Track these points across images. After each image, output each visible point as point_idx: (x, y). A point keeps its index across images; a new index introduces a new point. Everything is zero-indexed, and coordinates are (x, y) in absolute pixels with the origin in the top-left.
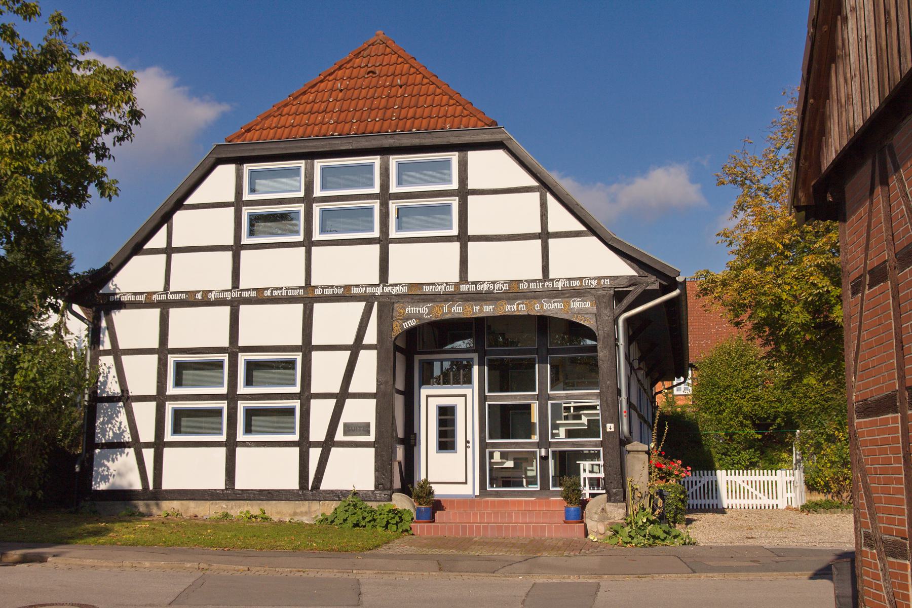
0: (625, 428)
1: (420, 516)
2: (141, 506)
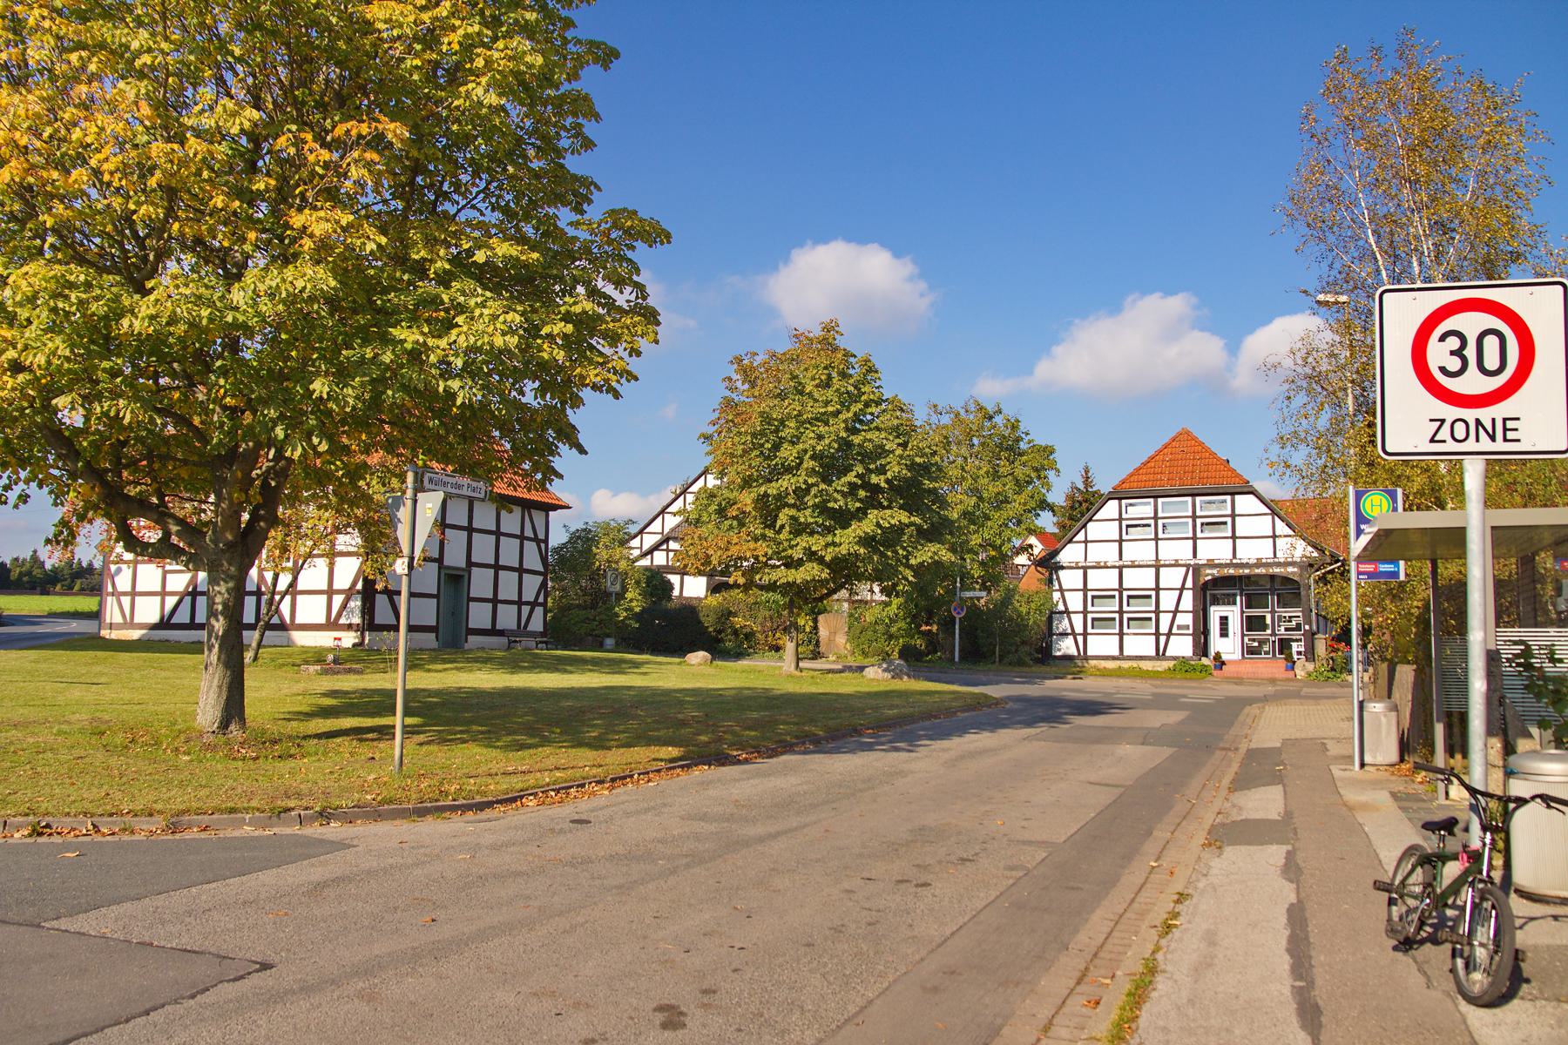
0: (1314, 628)
1: (1215, 666)
2: (1079, 663)
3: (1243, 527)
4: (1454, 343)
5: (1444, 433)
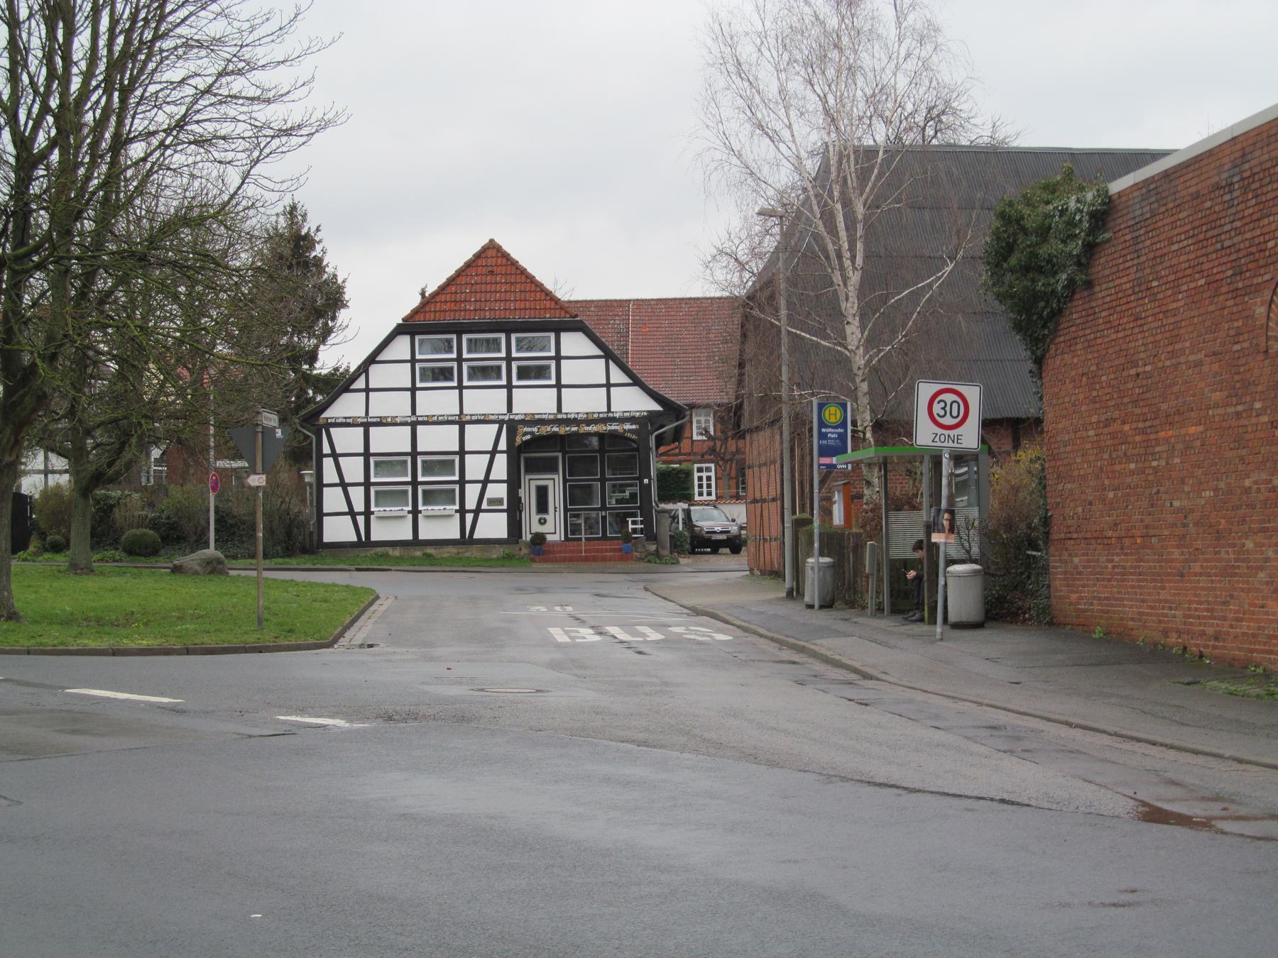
3: (570, 372)
4: (942, 405)
5: (937, 439)
